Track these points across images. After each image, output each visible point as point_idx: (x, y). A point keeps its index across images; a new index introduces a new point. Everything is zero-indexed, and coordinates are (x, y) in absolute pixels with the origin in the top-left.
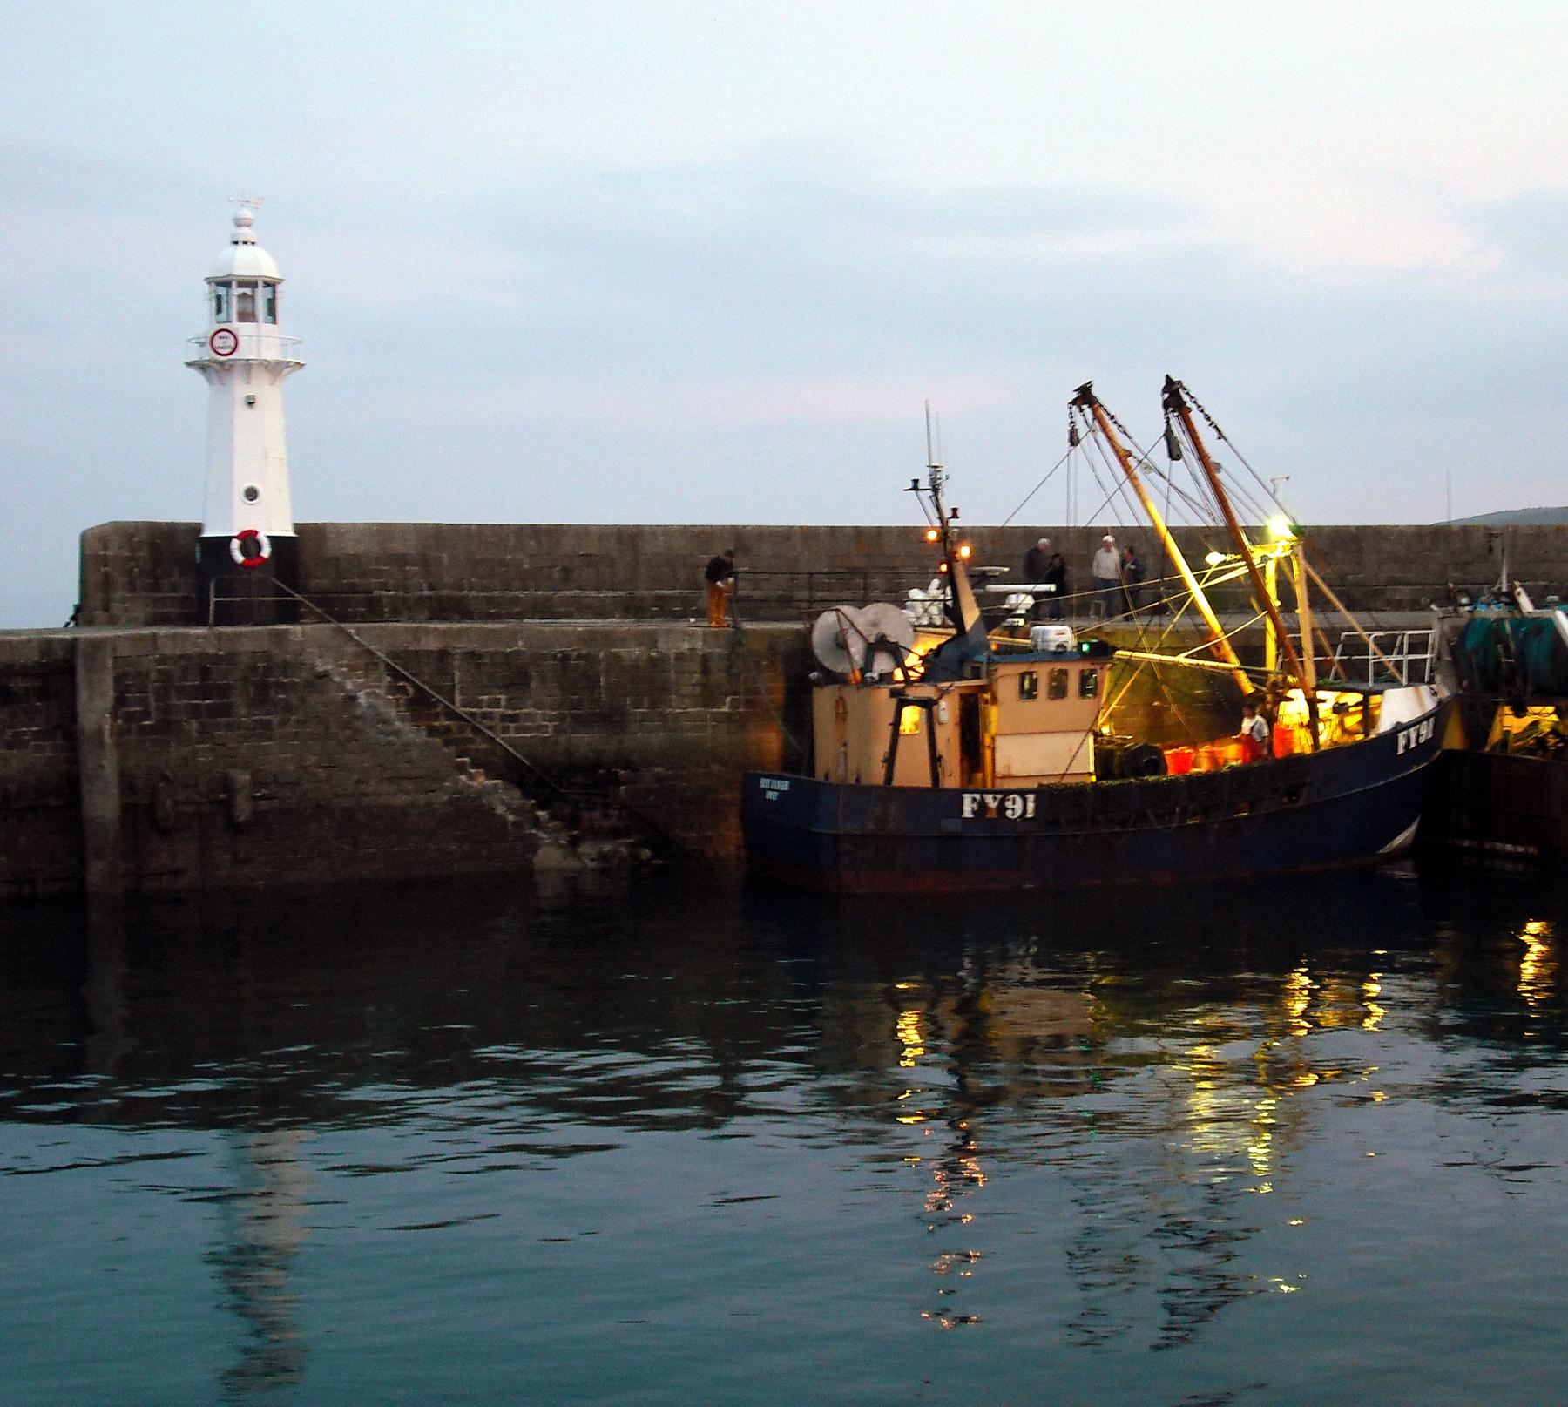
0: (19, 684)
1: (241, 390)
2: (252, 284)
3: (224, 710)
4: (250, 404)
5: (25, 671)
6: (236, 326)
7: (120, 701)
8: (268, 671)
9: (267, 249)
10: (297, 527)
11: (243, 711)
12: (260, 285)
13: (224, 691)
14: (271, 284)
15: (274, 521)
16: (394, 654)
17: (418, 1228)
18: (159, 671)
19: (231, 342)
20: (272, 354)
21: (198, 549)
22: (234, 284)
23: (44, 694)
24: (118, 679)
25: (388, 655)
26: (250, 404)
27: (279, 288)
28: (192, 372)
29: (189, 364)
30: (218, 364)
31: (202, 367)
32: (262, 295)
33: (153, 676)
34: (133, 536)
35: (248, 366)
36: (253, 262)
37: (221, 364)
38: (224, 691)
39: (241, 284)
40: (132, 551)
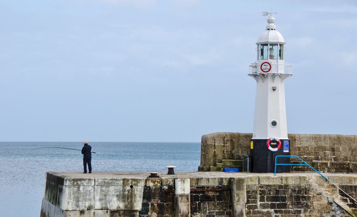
0: (211, 194)
1: (270, 84)
2: (273, 45)
3: (285, 206)
4: (274, 90)
5: (213, 189)
6: (269, 61)
7: (248, 202)
8: (299, 192)
9: (278, 31)
10: (289, 136)
11: (291, 206)
12: (278, 45)
13: (284, 199)
14: (281, 45)
15: (280, 134)
16: (342, 187)
17: (97, 210)
18: (260, 191)
19: (268, 67)
20: (281, 71)
21: (252, 144)
22: (269, 45)
23: (219, 198)
24: (248, 192)
25: (340, 187)
26: (274, 90)
27: (284, 46)
28: (250, 77)
29: (248, 75)
30: (262, 74)
31: (255, 76)
32: (276, 49)
33: (258, 192)
34: (224, 138)
35: (274, 76)
36: (276, 36)
37: (263, 75)
38: (284, 199)
39: (271, 45)
40: (224, 143)
